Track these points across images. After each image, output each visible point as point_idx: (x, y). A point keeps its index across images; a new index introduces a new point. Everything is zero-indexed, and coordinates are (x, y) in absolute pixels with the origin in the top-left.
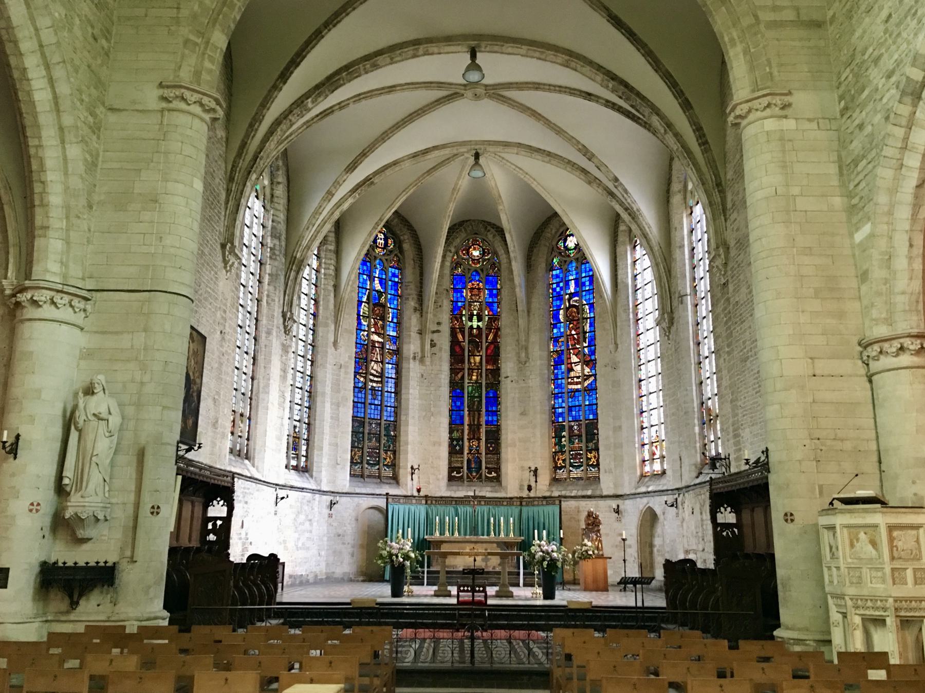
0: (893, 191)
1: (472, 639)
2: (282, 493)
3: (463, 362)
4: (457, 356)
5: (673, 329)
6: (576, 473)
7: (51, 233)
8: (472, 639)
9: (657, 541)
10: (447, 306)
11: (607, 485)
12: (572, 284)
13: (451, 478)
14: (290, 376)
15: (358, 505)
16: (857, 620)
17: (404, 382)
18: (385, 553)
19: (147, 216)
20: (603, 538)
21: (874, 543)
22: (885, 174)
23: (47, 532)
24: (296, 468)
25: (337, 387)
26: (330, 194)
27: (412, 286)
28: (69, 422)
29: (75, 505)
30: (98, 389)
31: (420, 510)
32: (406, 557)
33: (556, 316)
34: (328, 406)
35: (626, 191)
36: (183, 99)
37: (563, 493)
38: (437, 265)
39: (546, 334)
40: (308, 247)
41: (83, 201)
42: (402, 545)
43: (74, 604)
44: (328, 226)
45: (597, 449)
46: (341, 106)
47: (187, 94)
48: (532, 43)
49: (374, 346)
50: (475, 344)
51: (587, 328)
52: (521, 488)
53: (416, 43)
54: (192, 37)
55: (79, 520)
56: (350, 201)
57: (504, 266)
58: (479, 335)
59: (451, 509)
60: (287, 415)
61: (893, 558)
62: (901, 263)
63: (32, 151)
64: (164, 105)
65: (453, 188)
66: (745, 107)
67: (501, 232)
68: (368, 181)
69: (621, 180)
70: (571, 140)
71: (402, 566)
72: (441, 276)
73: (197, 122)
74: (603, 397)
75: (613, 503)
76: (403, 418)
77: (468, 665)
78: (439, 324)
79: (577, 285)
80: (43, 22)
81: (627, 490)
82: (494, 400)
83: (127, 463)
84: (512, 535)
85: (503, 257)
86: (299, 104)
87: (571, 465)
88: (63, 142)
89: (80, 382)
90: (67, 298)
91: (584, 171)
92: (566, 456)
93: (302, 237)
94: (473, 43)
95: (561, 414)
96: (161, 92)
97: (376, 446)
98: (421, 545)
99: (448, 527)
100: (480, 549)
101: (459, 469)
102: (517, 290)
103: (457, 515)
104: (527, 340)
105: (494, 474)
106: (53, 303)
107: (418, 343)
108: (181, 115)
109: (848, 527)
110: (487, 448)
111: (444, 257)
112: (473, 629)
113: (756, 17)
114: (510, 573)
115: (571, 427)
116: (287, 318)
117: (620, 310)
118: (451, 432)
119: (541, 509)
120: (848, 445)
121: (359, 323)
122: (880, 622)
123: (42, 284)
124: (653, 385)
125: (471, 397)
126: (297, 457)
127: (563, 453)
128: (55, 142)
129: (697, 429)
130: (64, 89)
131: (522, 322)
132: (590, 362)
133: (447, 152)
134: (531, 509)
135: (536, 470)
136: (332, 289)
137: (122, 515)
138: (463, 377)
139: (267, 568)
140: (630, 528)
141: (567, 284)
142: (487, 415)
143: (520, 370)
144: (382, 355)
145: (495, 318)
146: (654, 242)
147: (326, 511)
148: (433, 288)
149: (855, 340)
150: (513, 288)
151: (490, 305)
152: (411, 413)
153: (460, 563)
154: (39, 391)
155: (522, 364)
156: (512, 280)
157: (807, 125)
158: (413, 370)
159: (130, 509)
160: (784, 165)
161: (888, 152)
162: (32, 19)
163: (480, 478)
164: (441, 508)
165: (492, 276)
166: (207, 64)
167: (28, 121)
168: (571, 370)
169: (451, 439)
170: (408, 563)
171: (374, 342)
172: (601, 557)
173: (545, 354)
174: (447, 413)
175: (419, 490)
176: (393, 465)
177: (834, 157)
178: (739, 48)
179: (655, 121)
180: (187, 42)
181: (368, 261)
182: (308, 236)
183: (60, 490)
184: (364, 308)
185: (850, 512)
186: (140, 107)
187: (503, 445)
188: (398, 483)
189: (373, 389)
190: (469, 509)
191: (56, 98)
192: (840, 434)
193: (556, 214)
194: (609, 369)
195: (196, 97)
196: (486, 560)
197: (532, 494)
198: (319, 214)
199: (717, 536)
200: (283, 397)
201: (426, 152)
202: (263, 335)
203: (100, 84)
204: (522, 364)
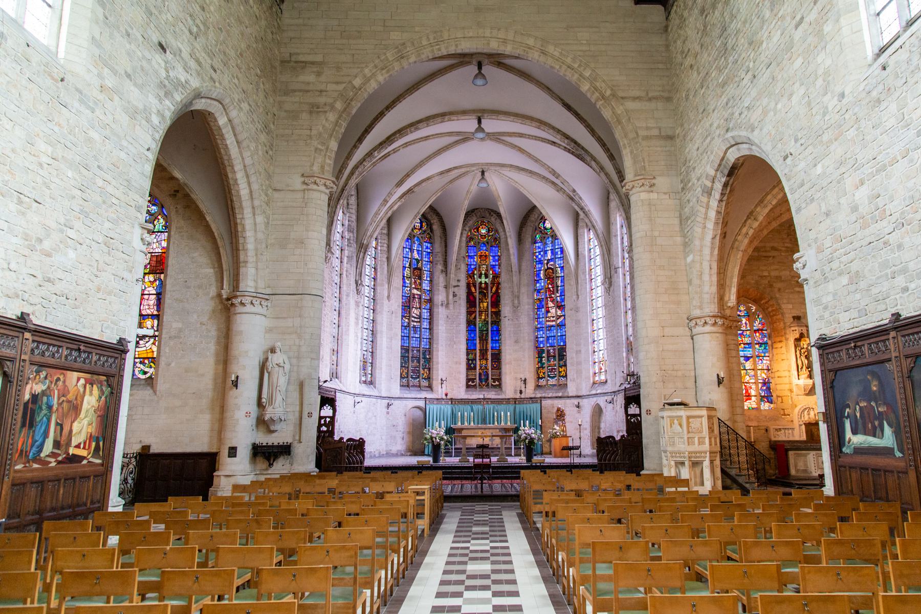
0: (702, 239)
1: (482, 483)
2: (358, 399)
3: (475, 307)
4: (471, 302)
5: (612, 289)
6: (552, 382)
7: (249, 265)
8: (482, 483)
9: (602, 425)
10: (463, 268)
11: (572, 390)
12: (549, 253)
13: (468, 386)
14: (360, 322)
15: (406, 406)
16: (673, 463)
17: (435, 322)
18: (428, 436)
19: (298, 251)
20: (567, 424)
21: (680, 425)
22: (698, 230)
23: (254, 427)
24: (365, 382)
25: (390, 327)
26: (386, 201)
27: (440, 255)
28: (263, 368)
29: (269, 413)
30: (278, 350)
31: (447, 408)
32: (442, 439)
33: (538, 275)
34: (385, 339)
35: (581, 198)
36: (315, 183)
37: (543, 395)
38: (457, 242)
39: (532, 289)
40: (371, 236)
41: (264, 246)
42: (437, 431)
43: (271, 465)
44: (384, 221)
45: (565, 365)
46: (395, 151)
47: (318, 180)
48: (516, 115)
49: (414, 298)
50: (484, 295)
51: (559, 283)
52: (515, 392)
53: (443, 115)
54: (320, 147)
55: (272, 420)
56: (399, 204)
57: (502, 240)
58: (486, 288)
59: (469, 408)
60: (359, 347)
61: (689, 432)
62: (706, 277)
63: (238, 221)
64: (305, 187)
65: (466, 192)
66: (631, 184)
67: (499, 215)
68: (410, 191)
69: (578, 191)
70: (544, 165)
71: (439, 445)
72: (460, 247)
73: (323, 195)
74: (570, 330)
75: (576, 401)
76: (435, 346)
77: (480, 493)
78: (458, 281)
79: (552, 253)
80: (246, 154)
81: (584, 393)
82: (497, 332)
83: (294, 388)
84: (509, 423)
85: (502, 234)
86: (370, 154)
87: (549, 376)
88: (254, 215)
89: (266, 345)
90: (259, 300)
91: (553, 183)
92: (545, 370)
93: (367, 230)
94: (480, 115)
95: (542, 342)
96: (303, 179)
97: (417, 365)
98: (449, 431)
99: (466, 419)
100: (489, 433)
101: (473, 380)
102: (512, 257)
103: (472, 410)
104: (519, 292)
105: (497, 383)
106: (252, 303)
107: (444, 294)
108: (315, 193)
109: (669, 417)
110: (492, 365)
111: (462, 234)
112: (482, 479)
113: (637, 133)
114: (506, 448)
115: (548, 351)
116: (358, 284)
117: (580, 273)
118: (468, 355)
119: (528, 406)
120: (680, 373)
121: (404, 282)
122: (683, 463)
123: (246, 294)
124: (601, 323)
125: (481, 331)
126: (366, 375)
127: (543, 368)
128: (251, 215)
129: (624, 354)
130: (255, 187)
131: (515, 279)
132: (561, 307)
133: (463, 170)
134: (522, 406)
135: (525, 380)
136: (385, 260)
137: (293, 417)
138: (475, 318)
139: (358, 446)
140: (585, 417)
141: (546, 252)
142: (492, 343)
143: (514, 311)
144: (420, 303)
145: (496, 276)
146: (599, 232)
147: (385, 410)
148: (454, 257)
149: (685, 316)
150: (509, 255)
151: (493, 267)
152: (440, 342)
153: (474, 442)
154: (247, 352)
155: (515, 308)
156: (508, 250)
157: (664, 197)
158: (441, 313)
159: (297, 414)
160: (650, 219)
161: (698, 219)
162: (241, 153)
163: (488, 385)
164: (461, 407)
165: (495, 241)
166: (328, 161)
167: (236, 205)
168: (548, 311)
169: (468, 360)
170: (442, 442)
171: (414, 295)
172: (566, 436)
173: (531, 301)
174: (465, 342)
175: (446, 395)
176: (429, 378)
177: (677, 214)
178: (628, 150)
179: (593, 163)
180: (316, 149)
181: (410, 238)
182: (371, 229)
183: (260, 404)
184: (407, 272)
185: (670, 409)
186: (290, 188)
187: (503, 363)
188: (432, 390)
189: (414, 327)
190: (480, 407)
191: (251, 192)
192: (676, 367)
193: (535, 207)
194: (573, 312)
195: (323, 181)
196: (492, 440)
197: (523, 396)
198: (377, 212)
199: (628, 421)
200: (357, 336)
201: (449, 170)
202: (344, 297)
203: (269, 177)
204: (515, 308)
